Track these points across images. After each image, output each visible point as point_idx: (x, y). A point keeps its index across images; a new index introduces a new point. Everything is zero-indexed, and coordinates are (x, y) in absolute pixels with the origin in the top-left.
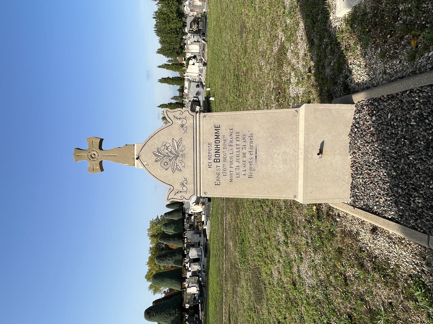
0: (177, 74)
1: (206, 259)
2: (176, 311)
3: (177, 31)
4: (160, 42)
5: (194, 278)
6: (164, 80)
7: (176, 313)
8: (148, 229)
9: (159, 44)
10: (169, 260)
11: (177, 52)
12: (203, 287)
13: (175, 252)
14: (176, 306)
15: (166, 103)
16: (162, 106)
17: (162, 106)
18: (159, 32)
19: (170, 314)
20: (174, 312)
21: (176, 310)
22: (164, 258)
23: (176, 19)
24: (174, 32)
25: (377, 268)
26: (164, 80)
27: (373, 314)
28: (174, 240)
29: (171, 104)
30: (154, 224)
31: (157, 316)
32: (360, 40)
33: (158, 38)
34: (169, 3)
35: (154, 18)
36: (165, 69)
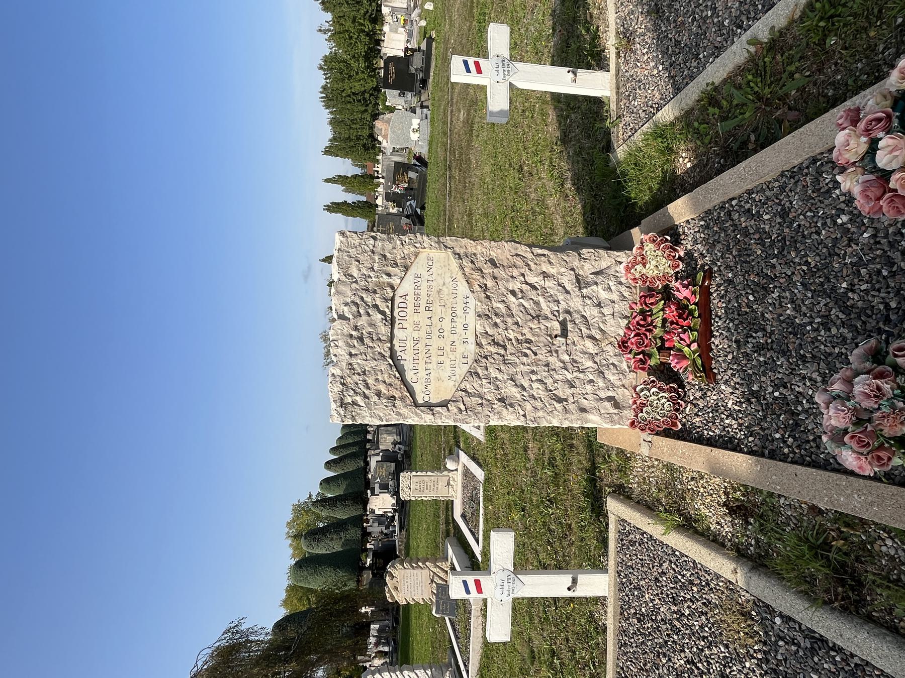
3: (364, 99)
4: (331, 123)
5: (385, 464)
6: (336, 207)
8: (288, 523)
10: (332, 539)
11: (364, 145)
13: (346, 523)
18: (331, 97)
22: (323, 537)
23: (363, 72)
24: (359, 101)
25: (592, 451)
26: (336, 207)
30: (300, 510)
33: (325, 115)
34: (351, 38)
35: (321, 68)
36: (339, 216)
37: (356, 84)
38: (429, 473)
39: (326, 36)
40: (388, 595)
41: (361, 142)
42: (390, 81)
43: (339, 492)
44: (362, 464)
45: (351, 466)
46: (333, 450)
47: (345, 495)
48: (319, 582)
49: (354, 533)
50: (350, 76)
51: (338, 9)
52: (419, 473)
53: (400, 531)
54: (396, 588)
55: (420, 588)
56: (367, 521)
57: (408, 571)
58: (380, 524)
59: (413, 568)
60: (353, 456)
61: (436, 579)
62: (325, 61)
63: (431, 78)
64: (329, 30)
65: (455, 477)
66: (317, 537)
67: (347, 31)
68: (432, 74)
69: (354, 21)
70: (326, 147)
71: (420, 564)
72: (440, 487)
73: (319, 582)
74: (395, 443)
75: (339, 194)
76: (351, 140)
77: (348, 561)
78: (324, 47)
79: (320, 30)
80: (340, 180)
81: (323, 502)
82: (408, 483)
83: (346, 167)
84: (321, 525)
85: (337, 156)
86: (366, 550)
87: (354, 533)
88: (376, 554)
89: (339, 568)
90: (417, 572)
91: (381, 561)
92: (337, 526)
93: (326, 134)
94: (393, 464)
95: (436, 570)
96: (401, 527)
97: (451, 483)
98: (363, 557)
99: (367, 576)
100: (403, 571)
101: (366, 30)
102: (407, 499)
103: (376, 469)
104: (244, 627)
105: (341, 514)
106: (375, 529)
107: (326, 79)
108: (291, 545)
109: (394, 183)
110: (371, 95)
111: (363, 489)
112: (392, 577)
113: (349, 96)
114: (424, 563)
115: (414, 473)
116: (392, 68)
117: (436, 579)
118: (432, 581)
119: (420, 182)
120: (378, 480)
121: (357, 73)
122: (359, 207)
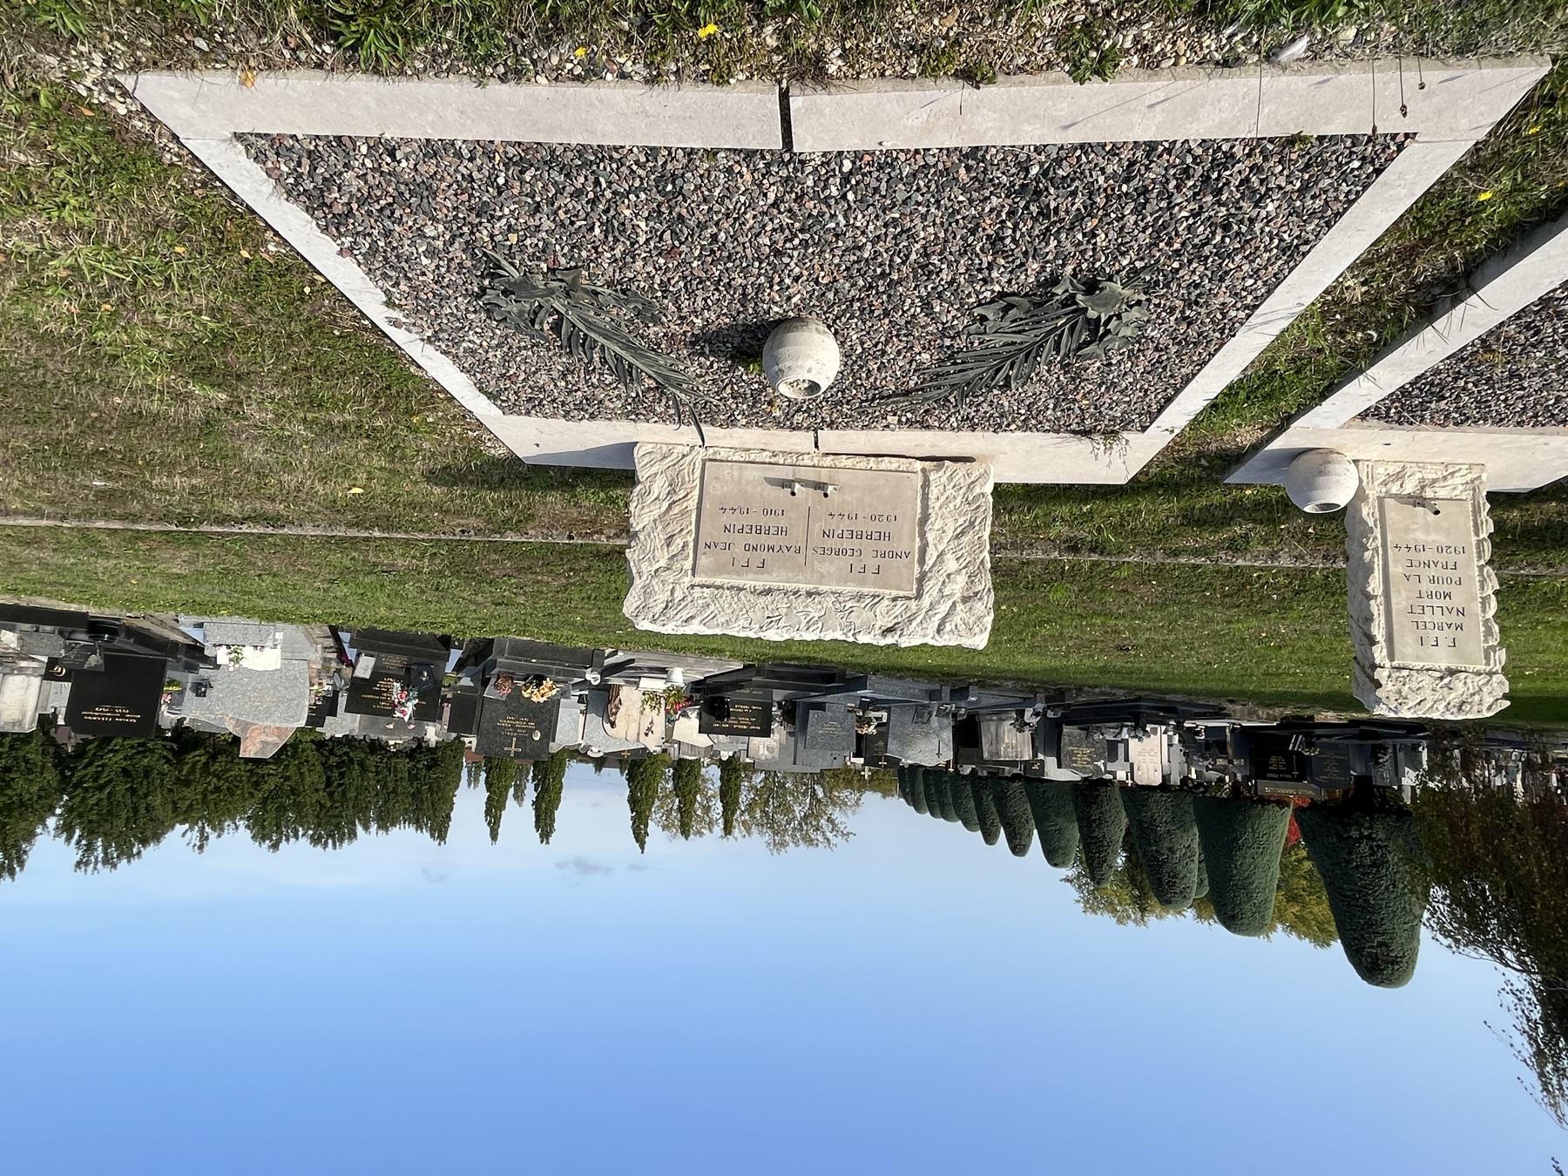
2: (1362, 837)
3: (339, 766)
5: (1067, 747)
6: (544, 823)
7: (1369, 837)
8: (1120, 922)
10: (1171, 850)
11: (429, 768)
13: (1140, 822)
14: (1340, 837)
16: (640, 836)
17: (640, 836)
19: (1374, 864)
20: (1364, 848)
21: (1355, 834)
24: (342, 775)
26: (544, 823)
27: (859, 5)
28: (1100, 822)
29: (633, 801)
30: (1095, 901)
31: (1388, 925)
33: (178, 838)
35: (275, 846)
37: (308, 780)
38: (1375, 585)
39: (213, 836)
42: (133, 718)
43: (1074, 833)
44: (1017, 784)
46: (990, 838)
47: (1079, 820)
50: (293, 791)
51: (160, 813)
52: (1378, 631)
60: (1001, 801)
62: (263, 839)
63: (84, 609)
64: (202, 830)
66: (1166, 879)
67: (205, 796)
68: (73, 607)
69: (187, 783)
70: (432, 836)
72: (1442, 540)
74: (1021, 725)
75: (519, 814)
76: (419, 791)
78: (236, 839)
79: (201, 847)
80: (494, 811)
82: (1427, 680)
83: (469, 799)
85: (448, 817)
89: (1236, 839)
91: (1273, 759)
93: (407, 838)
94: (1066, 729)
96: (1219, 713)
97: (1410, 487)
101: (203, 759)
102: (1501, 685)
105: (1119, 823)
107: (296, 836)
109: (390, 713)
110: (331, 752)
113: (331, 794)
115: (1380, 654)
116: (100, 714)
119: (381, 649)
120: (1100, 764)
121: (287, 779)
122: (544, 777)
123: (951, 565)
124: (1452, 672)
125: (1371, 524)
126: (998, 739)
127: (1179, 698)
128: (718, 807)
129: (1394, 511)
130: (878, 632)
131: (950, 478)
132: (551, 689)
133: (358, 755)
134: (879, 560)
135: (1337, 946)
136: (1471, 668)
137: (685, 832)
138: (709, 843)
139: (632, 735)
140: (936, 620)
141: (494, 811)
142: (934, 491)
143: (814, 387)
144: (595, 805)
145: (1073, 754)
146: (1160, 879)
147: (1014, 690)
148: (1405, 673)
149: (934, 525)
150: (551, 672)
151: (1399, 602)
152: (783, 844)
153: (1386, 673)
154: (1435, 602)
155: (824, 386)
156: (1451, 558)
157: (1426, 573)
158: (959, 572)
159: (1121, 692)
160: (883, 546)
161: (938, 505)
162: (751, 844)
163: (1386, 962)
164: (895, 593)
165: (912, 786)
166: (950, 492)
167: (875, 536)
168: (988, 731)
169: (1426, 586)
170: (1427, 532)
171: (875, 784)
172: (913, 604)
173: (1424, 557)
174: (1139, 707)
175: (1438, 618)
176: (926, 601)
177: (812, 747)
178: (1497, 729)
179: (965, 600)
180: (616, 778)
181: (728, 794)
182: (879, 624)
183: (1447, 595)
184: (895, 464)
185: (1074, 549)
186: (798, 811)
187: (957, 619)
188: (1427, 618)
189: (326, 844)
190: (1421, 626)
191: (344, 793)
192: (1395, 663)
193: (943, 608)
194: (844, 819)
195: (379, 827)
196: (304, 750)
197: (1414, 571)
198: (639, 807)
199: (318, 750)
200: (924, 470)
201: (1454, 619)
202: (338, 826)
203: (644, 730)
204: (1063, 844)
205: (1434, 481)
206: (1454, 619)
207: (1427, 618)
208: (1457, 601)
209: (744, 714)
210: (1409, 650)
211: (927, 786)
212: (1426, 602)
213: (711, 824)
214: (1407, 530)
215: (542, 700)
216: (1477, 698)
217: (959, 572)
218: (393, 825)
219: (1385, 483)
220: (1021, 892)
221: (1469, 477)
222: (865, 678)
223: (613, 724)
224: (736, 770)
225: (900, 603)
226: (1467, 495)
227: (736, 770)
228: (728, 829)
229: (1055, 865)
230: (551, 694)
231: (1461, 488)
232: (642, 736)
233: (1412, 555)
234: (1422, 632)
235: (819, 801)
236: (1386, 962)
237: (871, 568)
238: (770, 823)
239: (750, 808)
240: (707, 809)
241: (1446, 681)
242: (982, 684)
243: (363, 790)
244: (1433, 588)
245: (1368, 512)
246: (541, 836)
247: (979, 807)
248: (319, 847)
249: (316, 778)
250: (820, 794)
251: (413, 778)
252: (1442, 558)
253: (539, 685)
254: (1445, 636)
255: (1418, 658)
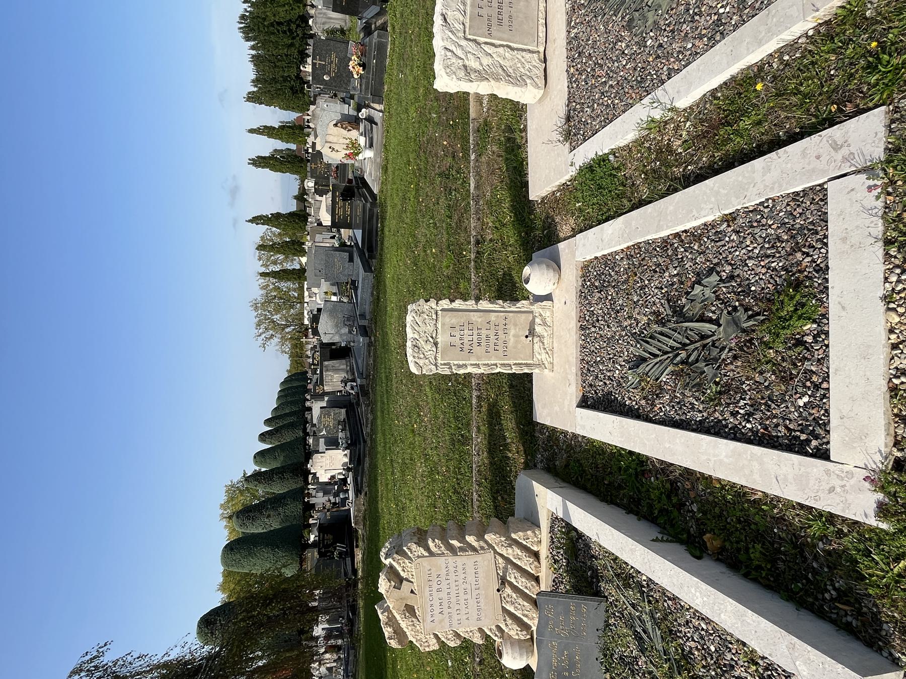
0: (290, 116)
1: (371, 276)
3: (290, 30)
5: (333, 412)
6: (260, 162)
8: (222, 505)
9: (220, 593)
10: (269, 516)
11: (292, 88)
12: (360, 462)
15: (268, 211)
16: (256, 220)
17: (256, 220)
24: (284, 32)
26: (260, 162)
28: (282, 479)
29: (277, 216)
30: (233, 491)
32: (782, 518)
37: (281, 9)
40: (387, 631)
41: (288, 84)
43: (275, 465)
44: (301, 434)
45: (288, 437)
46: (268, 422)
47: (283, 467)
48: (260, 565)
49: (294, 509)
52: (458, 304)
53: (357, 496)
54: (410, 610)
55: (472, 602)
56: (309, 495)
57: (442, 560)
58: (326, 493)
59: (453, 550)
60: (291, 426)
61: (513, 577)
65: (547, 314)
66: (251, 514)
71: (471, 539)
72: (512, 340)
73: (260, 565)
74: (345, 382)
75: (268, 146)
77: (290, 539)
80: (268, 131)
81: (257, 477)
82: (430, 328)
83: (275, 116)
84: (257, 502)
85: (261, 103)
86: (309, 525)
87: (294, 509)
88: (322, 529)
90: (466, 560)
91: (330, 537)
92: (275, 502)
94: (343, 411)
95: (512, 553)
97: (538, 329)
98: (305, 534)
99: (312, 555)
100: (426, 563)
103: (320, 418)
104: (108, 658)
105: (278, 489)
106: (319, 500)
108: (226, 527)
110: (298, 26)
111: (303, 460)
112: (398, 579)
113: (272, 25)
114: (480, 537)
115: (445, 304)
117: (513, 577)
118: (503, 581)
123: (486, 61)
124: (436, 344)
125: (518, 305)
126: (336, 370)
127: (367, 465)
128: (277, 268)
129: (524, 319)
130: (444, 11)
131: (535, 67)
132: (358, 73)
133: (297, 42)
134: (486, 17)
135: (219, 605)
136: (439, 355)
137: (261, 247)
138: (254, 264)
139: (330, 139)
140: (453, 48)
141: (268, 131)
142: (528, 56)
143: (527, 281)
144: (272, 198)
145: (329, 415)
146: (251, 511)
147: (368, 365)
148: (434, 317)
149: (508, 54)
150: (368, 73)
151: (475, 317)
152: (256, 309)
153: (434, 306)
154: (475, 337)
155: (528, 287)
156: (500, 348)
157: (492, 333)
158: (481, 64)
159: (369, 430)
160: (494, 21)
161: (520, 57)
162: (255, 289)
163: (212, 629)
164: (467, 25)
165: (296, 380)
166: (527, 66)
167: (500, 17)
168: (341, 364)
169: (484, 332)
170: (514, 336)
171: (297, 355)
172: (461, 34)
173: (500, 333)
174: (360, 444)
175: (466, 339)
176: (463, 43)
177: (327, 255)
178: (355, 656)
179: (465, 67)
180: (293, 207)
181: (283, 275)
182: (449, 13)
183: (479, 344)
184: (542, 35)
185: (478, 242)
186: (276, 317)
187: (454, 60)
188: (466, 331)
189: (241, 23)
190: (462, 328)
191: (273, 33)
192: (440, 312)
193: (459, 52)
194: (273, 344)
195: (253, 56)
196: (299, 7)
197: (493, 327)
198: (274, 219)
199: (299, 16)
200: (538, 52)
201: (466, 347)
202: (252, 30)
203: (333, 146)
204: (268, 461)
205: (543, 343)
206: (466, 347)
207: (466, 331)
208: (476, 349)
209: (345, 211)
210: (447, 320)
211: (296, 387)
212: (475, 332)
213: (267, 266)
214: (515, 325)
215: (350, 68)
216: (422, 356)
217: (481, 64)
218: (255, 65)
219: (541, 315)
220: (236, 448)
221: (546, 362)
222: (372, 272)
223: (336, 125)
224: (300, 278)
225: (461, 26)
226: (535, 361)
227: (300, 278)
228: (263, 275)
229: (255, 457)
230: (354, 73)
231: (539, 357)
232: (329, 145)
233: (502, 327)
234: (458, 328)
235: (283, 329)
236: (212, 629)
237: (481, 12)
238: (268, 301)
239: (277, 289)
240: (275, 263)
241: (431, 339)
242: (370, 344)
243: (276, 45)
244: (484, 336)
245: (523, 304)
246: (253, 160)
247: (286, 415)
248: (238, 20)
249: (282, 14)
250: (287, 330)
251: (285, 79)
252: (500, 342)
253: (359, 65)
254: (456, 341)
255: (443, 325)
